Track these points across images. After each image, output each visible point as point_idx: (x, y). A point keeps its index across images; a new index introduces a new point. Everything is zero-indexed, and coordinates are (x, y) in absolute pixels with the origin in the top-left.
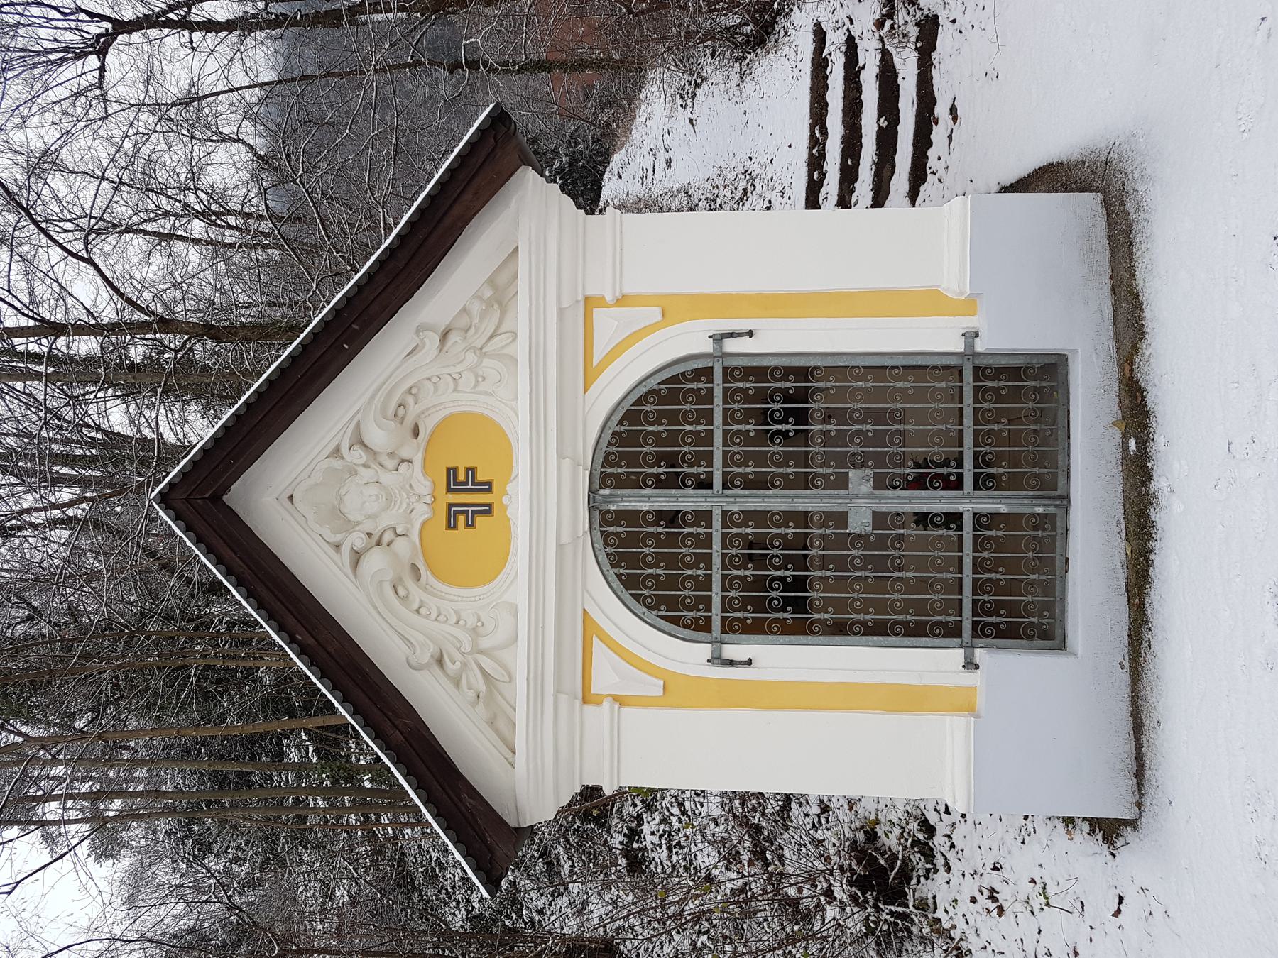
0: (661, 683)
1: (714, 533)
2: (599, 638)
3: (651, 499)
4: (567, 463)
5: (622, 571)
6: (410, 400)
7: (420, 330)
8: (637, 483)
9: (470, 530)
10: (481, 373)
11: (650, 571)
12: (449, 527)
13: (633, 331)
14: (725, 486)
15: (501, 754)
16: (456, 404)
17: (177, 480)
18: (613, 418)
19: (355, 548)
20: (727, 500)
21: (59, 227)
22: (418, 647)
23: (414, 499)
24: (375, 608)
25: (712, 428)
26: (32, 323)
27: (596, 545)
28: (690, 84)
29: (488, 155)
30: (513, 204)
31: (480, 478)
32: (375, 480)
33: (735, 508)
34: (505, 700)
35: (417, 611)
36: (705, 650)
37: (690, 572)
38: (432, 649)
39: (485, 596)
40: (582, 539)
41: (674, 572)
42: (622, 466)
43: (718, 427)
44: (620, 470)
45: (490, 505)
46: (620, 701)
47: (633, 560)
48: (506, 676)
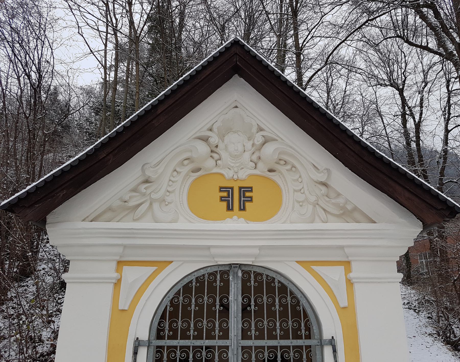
0: (126, 308)
1: (215, 341)
2: (156, 270)
3: (235, 302)
4: (256, 251)
5: (194, 284)
6: (289, 167)
7: (328, 170)
8: (245, 290)
9: (219, 199)
10: (304, 204)
11: (193, 300)
12: (221, 188)
13: (333, 289)
14: (243, 348)
15: (91, 214)
16: (287, 191)
17: (246, 48)
18: (282, 278)
19: (209, 138)
20: (235, 350)
21: (328, 72)
22: (155, 169)
23: (236, 169)
24: (177, 147)
25: (278, 339)
26: (300, 45)
27: (209, 268)
28: (415, 307)
29: (433, 206)
30: (402, 220)
31: (247, 204)
32: (246, 149)
33: (230, 354)
34: (124, 217)
35: (175, 170)
36: (144, 335)
37: (192, 325)
38: (153, 177)
39: (182, 207)
40: (213, 260)
41: (192, 316)
42: (280, 307)
43: (279, 343)
44: (252, 282)
45: (232, 209)
46: (118, 283)
47: (200, 290)
48: (137, 218)
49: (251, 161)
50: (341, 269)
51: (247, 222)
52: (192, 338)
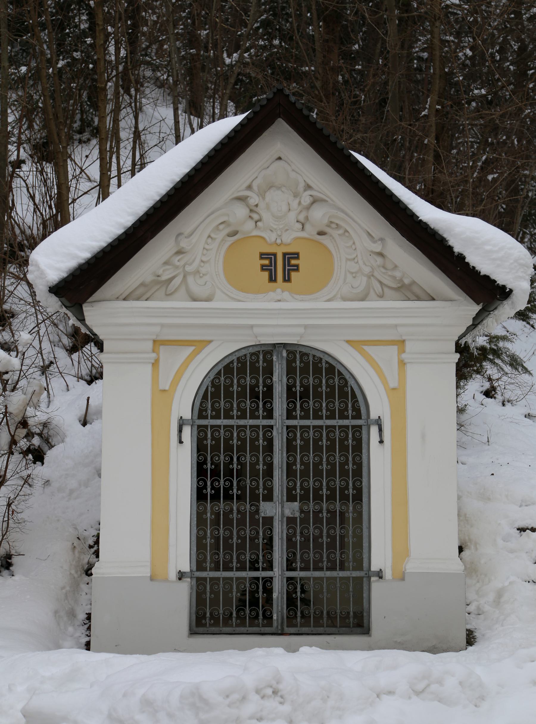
1: (259, 421)
2: (194, 350)
3: (280, 382)
4: (301, 330)
5: (235, 364)
6: (341, 232)
8: (290, 371)
9: (259, 268)
14: (288, 427)
18: (330, 358)
20: (280, 428)
23: (279, 233)
24: (212, 213)
31: (293, 274)
33: (275, 433)
36: (187, 415)
41: (235, 396)
43: (324, 423)
45: (275, 281)
46: (155, 364)
47: (242, 371)
48: (170, 292)
49: (297, 221)
50: (394, 349)
51: (293, 297)
52: (235, 417)
